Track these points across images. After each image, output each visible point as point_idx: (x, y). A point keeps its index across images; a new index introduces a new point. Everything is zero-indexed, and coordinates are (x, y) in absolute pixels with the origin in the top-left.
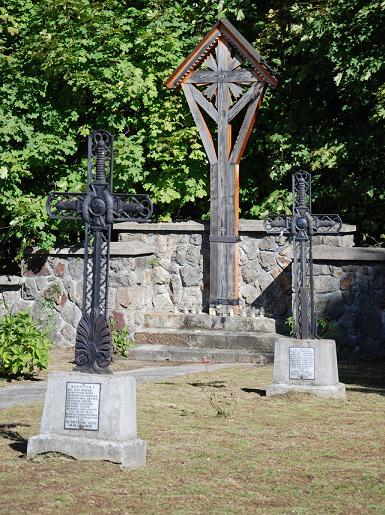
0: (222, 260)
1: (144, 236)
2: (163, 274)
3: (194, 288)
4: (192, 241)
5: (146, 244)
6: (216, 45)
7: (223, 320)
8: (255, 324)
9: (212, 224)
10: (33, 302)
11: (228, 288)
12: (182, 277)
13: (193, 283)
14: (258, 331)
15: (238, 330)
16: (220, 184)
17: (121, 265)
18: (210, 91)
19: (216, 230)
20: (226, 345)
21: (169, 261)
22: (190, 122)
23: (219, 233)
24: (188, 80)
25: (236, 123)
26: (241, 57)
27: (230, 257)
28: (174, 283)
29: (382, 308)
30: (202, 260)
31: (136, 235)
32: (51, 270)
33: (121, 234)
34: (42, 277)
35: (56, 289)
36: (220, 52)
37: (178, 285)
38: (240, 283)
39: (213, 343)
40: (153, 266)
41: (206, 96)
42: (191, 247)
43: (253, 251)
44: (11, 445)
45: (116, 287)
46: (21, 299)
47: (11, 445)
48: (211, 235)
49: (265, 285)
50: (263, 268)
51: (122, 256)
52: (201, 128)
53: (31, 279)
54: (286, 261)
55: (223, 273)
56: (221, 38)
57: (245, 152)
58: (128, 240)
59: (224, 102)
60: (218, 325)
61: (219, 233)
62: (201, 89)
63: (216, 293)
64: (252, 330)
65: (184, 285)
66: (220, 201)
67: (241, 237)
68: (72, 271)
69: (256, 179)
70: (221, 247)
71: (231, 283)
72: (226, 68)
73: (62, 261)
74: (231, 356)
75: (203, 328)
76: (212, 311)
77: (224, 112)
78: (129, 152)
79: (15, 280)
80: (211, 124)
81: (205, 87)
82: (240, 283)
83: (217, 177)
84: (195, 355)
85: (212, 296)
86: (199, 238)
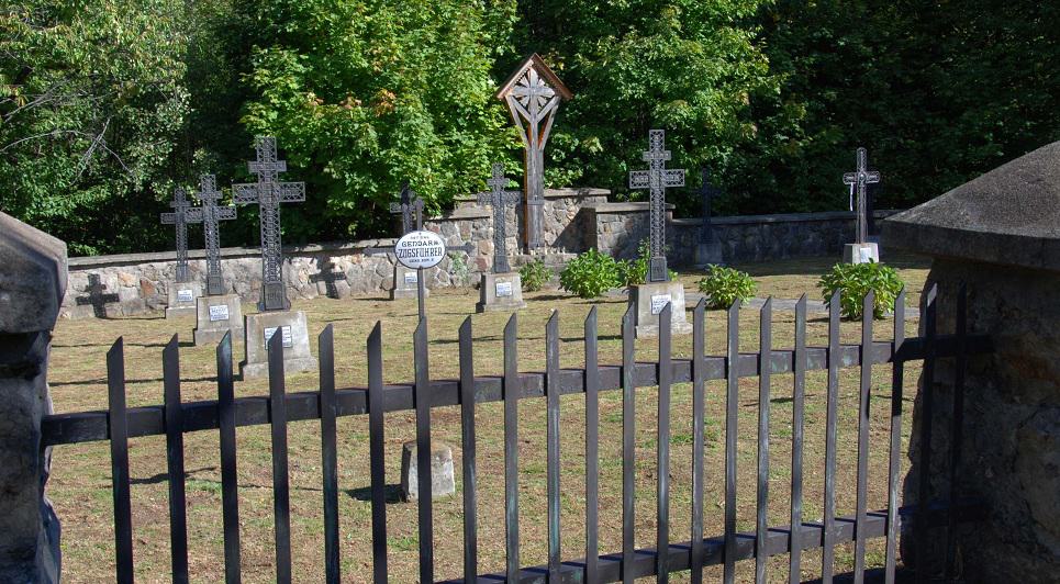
0: (536, 217)
18: (525, 102)
24: (510, 93)
49: (560, 232)
59: (534, 109)
62: (519, 99)
70: (535, 208)
80: (525, 124)
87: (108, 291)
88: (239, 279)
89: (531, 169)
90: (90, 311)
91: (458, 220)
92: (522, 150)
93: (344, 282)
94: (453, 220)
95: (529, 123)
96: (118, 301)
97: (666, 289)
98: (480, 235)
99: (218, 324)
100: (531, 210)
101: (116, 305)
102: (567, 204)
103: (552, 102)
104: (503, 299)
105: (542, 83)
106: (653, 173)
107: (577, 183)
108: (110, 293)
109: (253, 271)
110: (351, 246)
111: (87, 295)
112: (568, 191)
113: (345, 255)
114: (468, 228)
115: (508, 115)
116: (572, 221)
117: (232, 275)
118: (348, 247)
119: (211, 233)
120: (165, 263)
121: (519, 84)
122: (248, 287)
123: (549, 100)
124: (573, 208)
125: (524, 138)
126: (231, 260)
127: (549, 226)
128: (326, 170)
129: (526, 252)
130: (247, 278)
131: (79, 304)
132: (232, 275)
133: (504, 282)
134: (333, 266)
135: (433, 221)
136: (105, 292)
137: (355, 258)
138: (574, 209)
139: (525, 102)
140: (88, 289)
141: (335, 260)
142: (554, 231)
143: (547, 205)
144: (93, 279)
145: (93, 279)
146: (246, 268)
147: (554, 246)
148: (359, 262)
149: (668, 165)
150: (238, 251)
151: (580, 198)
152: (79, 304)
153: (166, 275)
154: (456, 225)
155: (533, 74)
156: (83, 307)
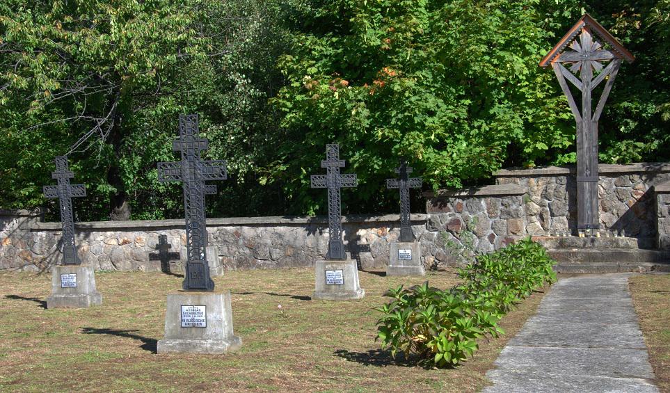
0: (587, 195)
1: (518, 180)
2: (535, 208)
3: (561, 218)
4: (558, 181)
5: (520, 186)
6: (580, 32)
7: (593, 241)
8: (620, 243)
9: (579, 168)
10: (436, 233)
11: (593, 216)
12: (551, 209)
13: (560, 213)
14: (623, 248)
15: (606, 247)
16: (584, 137)
17: (510, 202)
18: (575, 68)
19: (582, 173)
20: (602, 260)
21: (539, 198)
22: (559, 92)
23: (585, 175)
24: (557, 60)
25: (596, 94)
26: (601, 41)
27: (594, 192)
28: (544, 214)
29: (669, 225)
30: (567, 196)
31: (510, 179)
32: (451, 208)
33: (499, 179)
34: (444, 214)
35: (456, 222)
36: (584, 37)
37: (547, 216)
38: (600, 212)
39: (591, 258)
40: (526, 202)
41: (572, 72)
42: (559, 187)
43: (611, 187)
44: (142, 346)
45: (507, 219)
46: (426, 231)
47: (142, 346)
48: (578, 176)
49: (622, 213)
50: (620, 200)
51: (512, 195)
52: (567, 97)
53: (435, 215)
54: (640, 194)
55: (589, 204)
56: (585, 28)
57: (603, 116)
58: (505, 183)
59: (586, 76)
60: (589, 244)
61: (585, 175)
62: (567, 67)
63: (583, 221)
64: (618, 246)
65: (552, 215)
66: (585, 150)
67: (600, 178)
68: (469, 208)
69: (608, 132)
70: (587, 185)
71: (595, 212)
72: (589, 50)
73: (460, 201)
74: (613, 268)
75: (576, 247)
76: (582, 235)
77: (588, 82)
78: (509, 119)
79: (423, 217)
80: (577, 96)
81: (570, 65)
82: (600, 212)
83: (582, 132)
84: (582, 268)
85: (579, 223)
86: (564, 180)
87: (173, 250)
88: (274, 246)
89: (582, 142)
90: (158, 266)
91: (484, 196)
92: (572, 122)
93: (368, 254)
94: (479, 197)
95: (580, 93)
96: (179, 259)
97: (199, 299)
98: (509, 213)
99: (68, 290)
100: (583, 188)
101: (177, 262)
102: (632, 180)
103: (611, 66)
104: (333, 287)
105: (598, 45)
106: (330, 176)
107: (648, 157)
108: (174, 251)
109: (286, 238)
110: (372, 219)
111: (157, 252)
112: (638, 166)
113: (372, 228)
114: (495, 205)
115: (555, 82)
116: (639, 201)
117: (269, 242)
118: (370, 220)
119: (65, 208)
120: (216, 228)
121: (568, 49)
122: (282, 253)
123: (606, 64)
124: (641, 186)
125: (572, 107)
126: (268, 228)
127: (608, 205)
128: (35, 167)
129: (575, 233)
130: (281, 245)
131: (150, 260)
132: (269, 242)
133: (334, 270)
134: (359, 238)
135: (459, 197)
136: (170, 251)
137: (378, 231)
138: (642, 187)
139: (575, 68)
140: (158, 247)
141: (362, 232)
142: (615, 211)
143: (604, 184)
144: (162, 238)
145: (162, 238)
146: (280, 236)
147: (613, 228)
148: (383, 235)
149: (342, 170)
150: (274, 220)
151: (650, 175)
152: (150, 260)
153: (216, 238)
154: (483, 202)
155: (586, 36)
156: (153, 262)
